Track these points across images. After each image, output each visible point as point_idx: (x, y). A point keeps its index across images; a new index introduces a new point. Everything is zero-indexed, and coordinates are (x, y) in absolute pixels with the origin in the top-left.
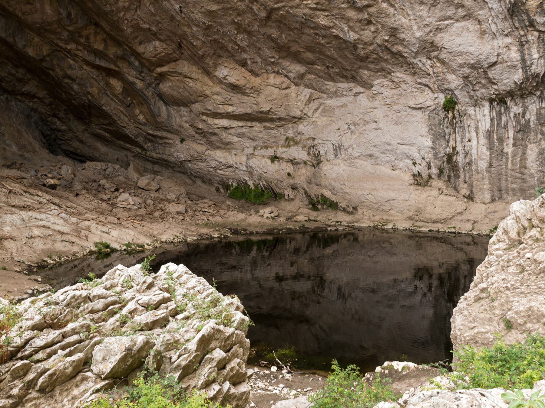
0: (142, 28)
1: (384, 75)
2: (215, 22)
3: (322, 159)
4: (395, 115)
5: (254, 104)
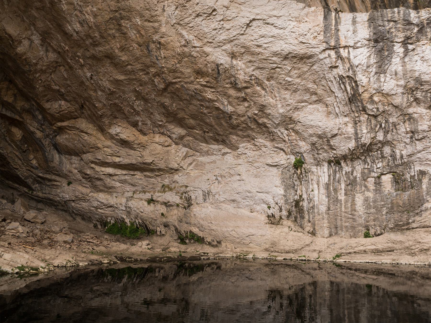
0: (53, 89)
1: (248, 141)
2: (119, 89)
3: (193, 202)
4: (255, 170)
5: (138, 156)
